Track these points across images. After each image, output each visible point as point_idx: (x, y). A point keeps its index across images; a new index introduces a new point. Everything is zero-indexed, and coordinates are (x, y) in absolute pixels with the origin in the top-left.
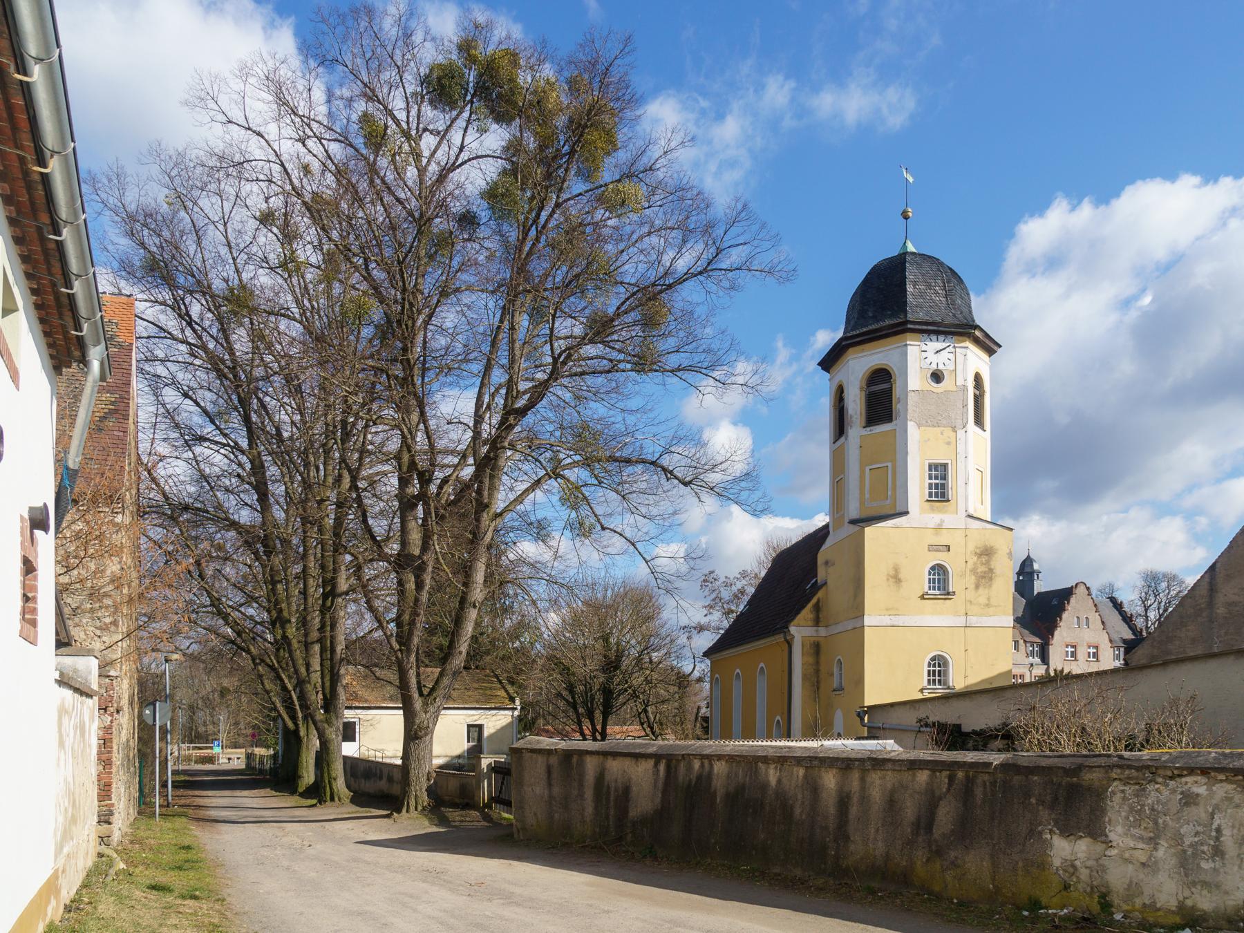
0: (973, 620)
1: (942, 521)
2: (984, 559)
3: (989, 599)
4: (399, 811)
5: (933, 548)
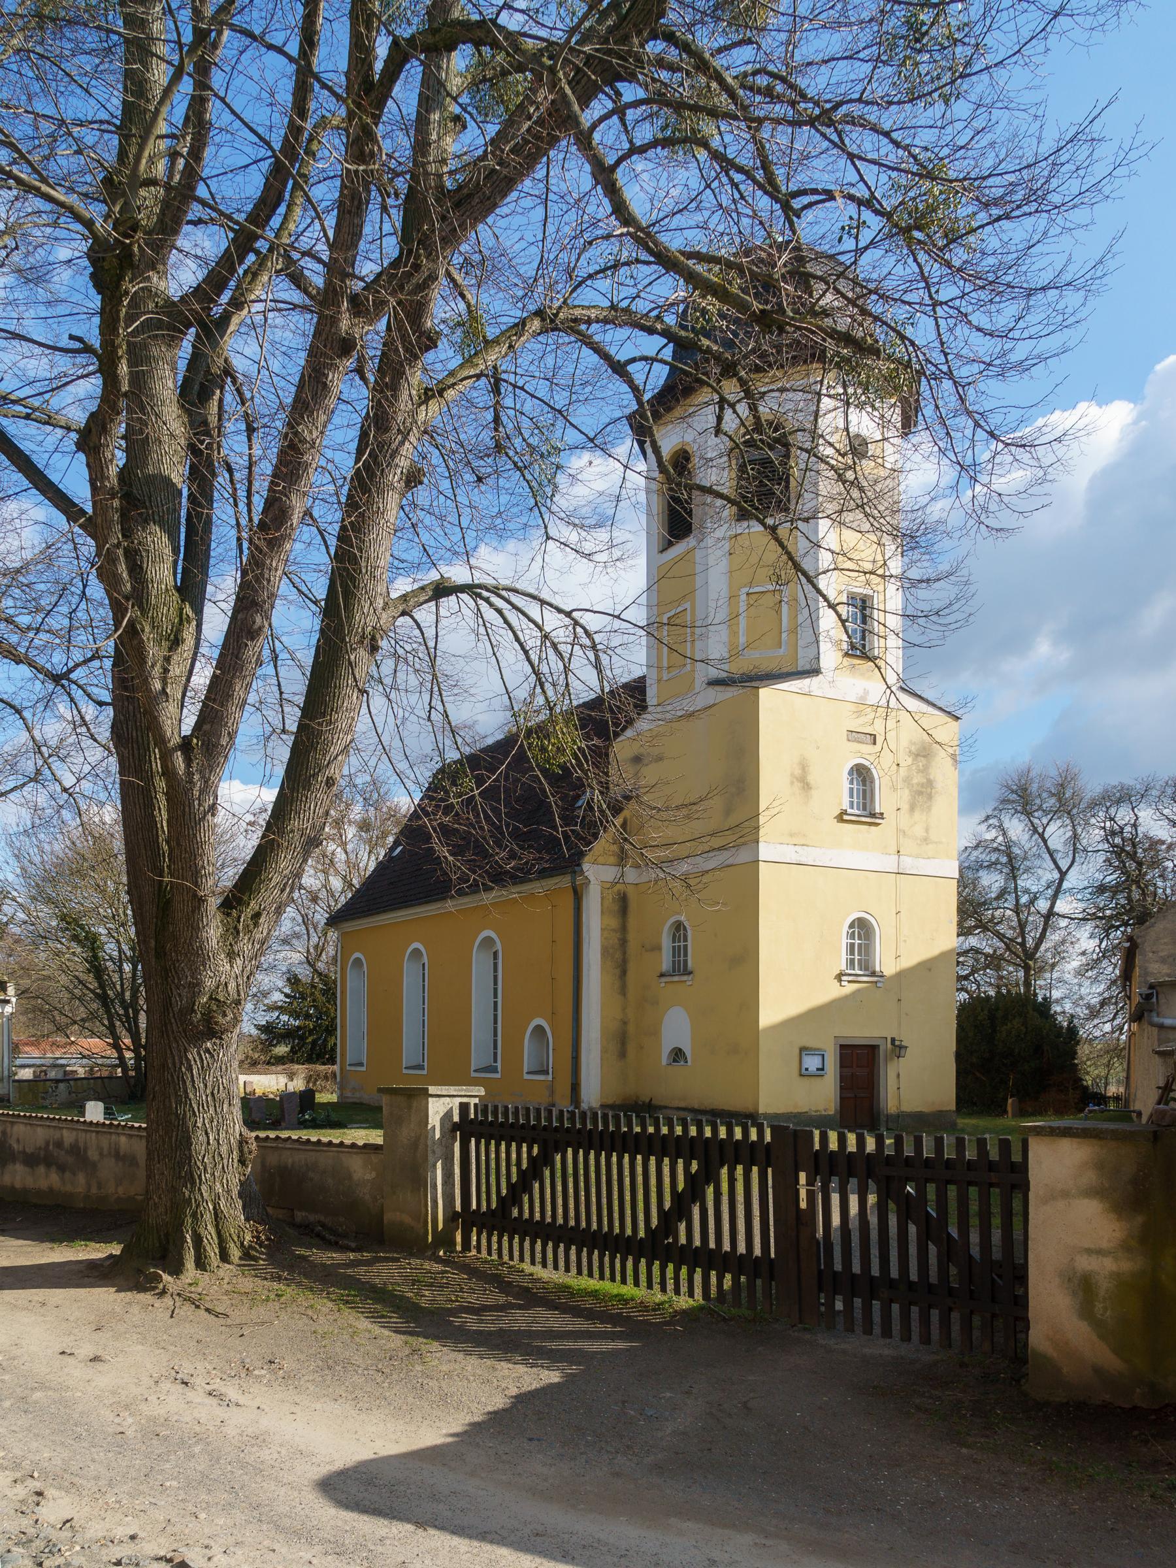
0: (908, 863)
1: (866, 692)
2: (922, 762)
3: (927, 830)
4: (176, 1270)
5: (854, 735)
